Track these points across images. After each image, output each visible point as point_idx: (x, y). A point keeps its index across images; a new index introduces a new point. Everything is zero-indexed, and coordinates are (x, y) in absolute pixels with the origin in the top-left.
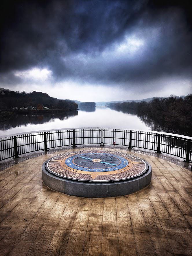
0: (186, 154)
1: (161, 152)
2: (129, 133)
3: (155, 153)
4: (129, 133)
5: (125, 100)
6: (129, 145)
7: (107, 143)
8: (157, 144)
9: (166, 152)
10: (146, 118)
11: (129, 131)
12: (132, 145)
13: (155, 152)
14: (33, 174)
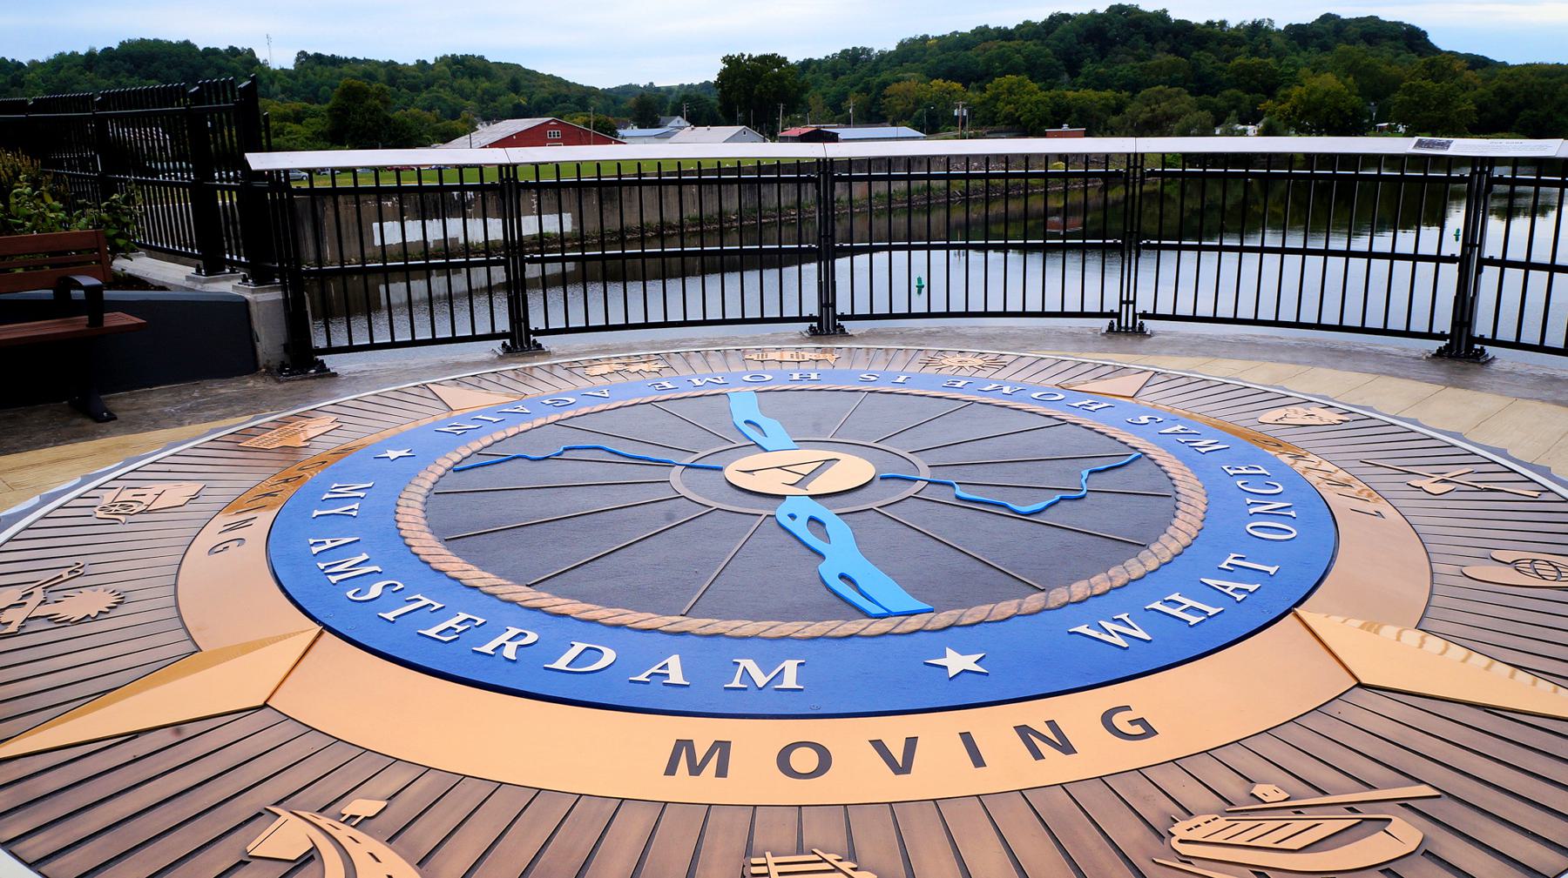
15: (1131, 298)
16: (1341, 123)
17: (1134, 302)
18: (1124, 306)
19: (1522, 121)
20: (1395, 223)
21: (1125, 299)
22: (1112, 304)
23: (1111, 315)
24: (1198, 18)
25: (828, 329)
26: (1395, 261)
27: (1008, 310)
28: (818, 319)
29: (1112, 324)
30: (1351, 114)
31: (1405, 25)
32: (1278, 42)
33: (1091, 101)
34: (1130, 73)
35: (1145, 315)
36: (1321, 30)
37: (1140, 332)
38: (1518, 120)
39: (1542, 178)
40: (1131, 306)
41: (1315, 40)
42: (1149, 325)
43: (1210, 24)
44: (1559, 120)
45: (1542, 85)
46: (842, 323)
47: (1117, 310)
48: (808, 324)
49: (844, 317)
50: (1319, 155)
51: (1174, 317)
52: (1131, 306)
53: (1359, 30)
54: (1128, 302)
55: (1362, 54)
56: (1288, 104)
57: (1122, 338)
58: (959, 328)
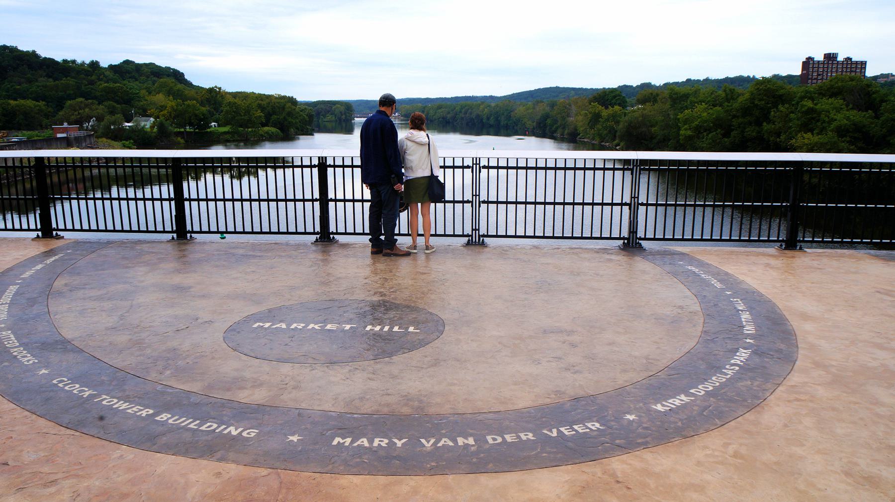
0: (174, 213)
1: (58, 230)
2: (315, 170)
3: (33, 239)
4: (315, 171)
5: (743, 75)
6: (318, 229)
7: (502, 232)
8: (186, 195)
9: (94, 227)
10: (791, 248)
11: (315, 162)
12: (332, 229)
13: (34, 234)
14: (196, 487)
15: (477, 228)
16: (198, 122)
17: (479, 230)
18: (474, 232)
19: (273, 121)
20: (36, 176)
21: (474, 228)
22: (468, 230)
23: (468, 236)
24: (59, 57)
25: (632, 244)
26: (518, 205)
27: (517, 235)
28: (628, 239)
29: (469, 240)
30: (202, 117)
31: (172, 69)
32: (109, 74)
33: (30, 107)
34: (38, 89)
35: (484, 236)
36: (130, 69)
37: (483, 244)
38: (271, 121)
39: (872, 170)
40: (477, 232)
41: (127, 74)
42: (486, 240)
43: (65, 61)
44: (290, 120)
45: (278, 103)
46: (640, 242)
47: (470, 234)
48: (622, 241)
49: (640, 239)
50: (650, 160)
51: (497, 236)
52: (477, 232)
53: (149, 70)
54: (476, 230)
55: (174, 84)
56: (166, 111)
57: (478, 247)
58: (518, 245)
